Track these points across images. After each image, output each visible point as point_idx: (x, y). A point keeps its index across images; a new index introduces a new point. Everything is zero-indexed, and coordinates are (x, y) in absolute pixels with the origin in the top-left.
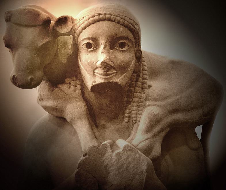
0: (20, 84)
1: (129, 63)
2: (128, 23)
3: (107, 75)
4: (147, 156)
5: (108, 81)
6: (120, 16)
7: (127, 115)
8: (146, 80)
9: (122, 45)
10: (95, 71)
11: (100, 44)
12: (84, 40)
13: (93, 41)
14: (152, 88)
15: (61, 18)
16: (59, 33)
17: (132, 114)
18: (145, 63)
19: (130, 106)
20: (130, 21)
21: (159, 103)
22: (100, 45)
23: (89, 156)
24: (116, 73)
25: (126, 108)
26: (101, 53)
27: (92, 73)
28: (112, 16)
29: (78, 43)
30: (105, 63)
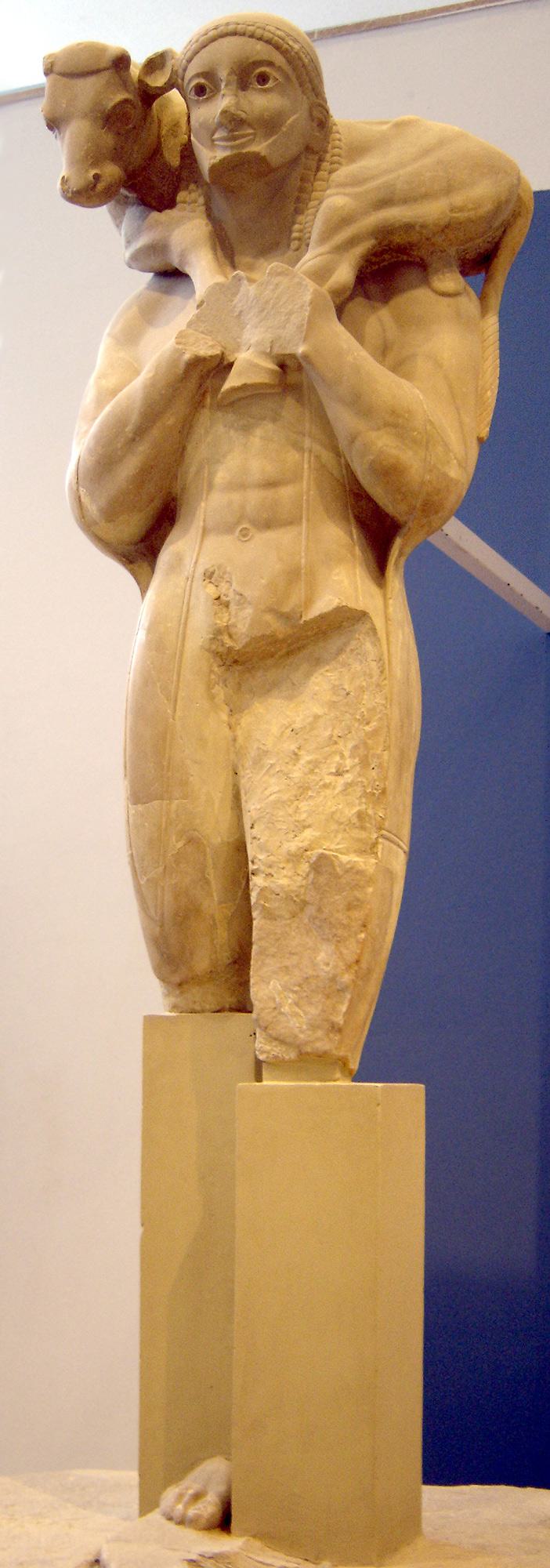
3: (234, 138)
5: (240, 151)
6: (257, 24)
9: (263, 79)
12: (190, 81)
13: (204, 78)
16: (151, 87)
21: (349, 190)
23: (208, 305)
24: (255, 134)
28: (240, 26)
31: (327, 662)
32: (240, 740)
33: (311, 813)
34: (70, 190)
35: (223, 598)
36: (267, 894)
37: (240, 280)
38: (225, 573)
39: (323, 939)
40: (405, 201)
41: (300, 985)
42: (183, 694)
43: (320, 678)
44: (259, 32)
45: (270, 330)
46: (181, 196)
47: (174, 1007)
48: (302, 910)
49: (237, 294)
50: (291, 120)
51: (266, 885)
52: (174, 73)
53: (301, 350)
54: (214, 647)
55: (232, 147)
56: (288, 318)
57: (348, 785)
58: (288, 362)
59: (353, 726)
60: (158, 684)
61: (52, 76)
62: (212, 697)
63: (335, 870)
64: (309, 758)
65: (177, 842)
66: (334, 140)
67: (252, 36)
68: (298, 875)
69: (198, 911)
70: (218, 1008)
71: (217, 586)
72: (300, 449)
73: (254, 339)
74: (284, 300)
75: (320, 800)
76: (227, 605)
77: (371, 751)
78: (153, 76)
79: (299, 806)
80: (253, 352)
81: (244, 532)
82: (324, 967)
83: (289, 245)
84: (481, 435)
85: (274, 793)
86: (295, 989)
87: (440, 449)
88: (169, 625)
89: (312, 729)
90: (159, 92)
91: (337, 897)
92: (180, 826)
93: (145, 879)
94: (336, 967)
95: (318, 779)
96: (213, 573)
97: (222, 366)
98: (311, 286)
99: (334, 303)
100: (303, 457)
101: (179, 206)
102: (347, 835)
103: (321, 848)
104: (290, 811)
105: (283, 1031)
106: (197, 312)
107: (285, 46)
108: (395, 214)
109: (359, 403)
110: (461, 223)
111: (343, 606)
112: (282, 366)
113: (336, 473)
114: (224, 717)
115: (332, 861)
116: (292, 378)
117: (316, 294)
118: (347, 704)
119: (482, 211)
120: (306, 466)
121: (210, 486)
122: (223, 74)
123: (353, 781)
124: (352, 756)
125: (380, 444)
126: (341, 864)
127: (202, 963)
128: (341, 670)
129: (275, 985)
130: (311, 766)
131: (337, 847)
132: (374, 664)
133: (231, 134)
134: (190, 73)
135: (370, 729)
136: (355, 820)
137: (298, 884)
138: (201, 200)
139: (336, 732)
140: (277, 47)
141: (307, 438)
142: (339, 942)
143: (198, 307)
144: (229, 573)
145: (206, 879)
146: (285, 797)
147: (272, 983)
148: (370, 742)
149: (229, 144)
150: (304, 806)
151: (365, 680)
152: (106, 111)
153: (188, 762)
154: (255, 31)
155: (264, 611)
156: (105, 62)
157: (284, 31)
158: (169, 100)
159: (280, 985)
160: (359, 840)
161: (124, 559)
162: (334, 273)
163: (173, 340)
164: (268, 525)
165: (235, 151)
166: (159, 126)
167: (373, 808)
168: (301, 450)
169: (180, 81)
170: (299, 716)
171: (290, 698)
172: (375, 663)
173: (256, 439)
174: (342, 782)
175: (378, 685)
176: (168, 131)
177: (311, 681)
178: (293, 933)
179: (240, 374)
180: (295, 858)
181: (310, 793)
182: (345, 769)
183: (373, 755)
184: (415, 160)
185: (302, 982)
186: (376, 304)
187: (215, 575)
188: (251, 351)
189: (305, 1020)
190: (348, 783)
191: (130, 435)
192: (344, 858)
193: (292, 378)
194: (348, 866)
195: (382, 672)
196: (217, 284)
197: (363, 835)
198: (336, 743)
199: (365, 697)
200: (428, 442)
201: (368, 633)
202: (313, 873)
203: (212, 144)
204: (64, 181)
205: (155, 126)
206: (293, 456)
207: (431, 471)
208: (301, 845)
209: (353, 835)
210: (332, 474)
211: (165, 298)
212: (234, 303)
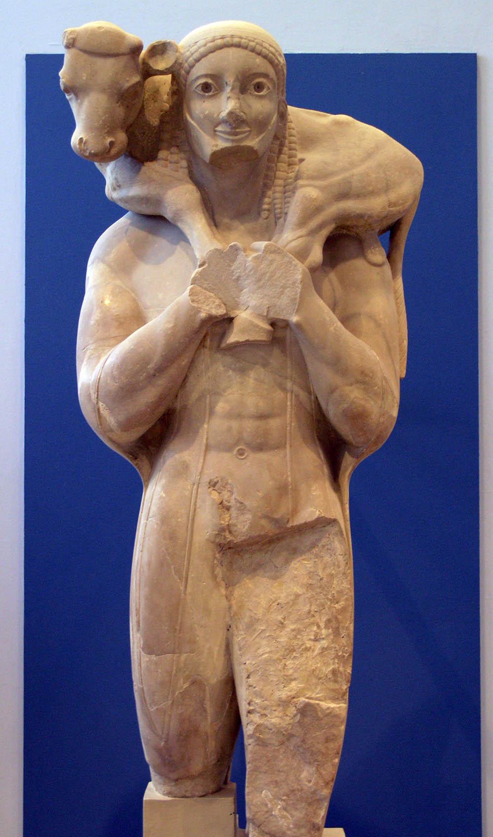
0: (93, 151)
1: (268, 118)
2: (268, 52)
3: (236, 134)
4: (303, 262)
5: (238, 144)
6: (256, 41)
8: (294, 151)
10: (216, 129)
11: (225, 84)
12: (198, 78)
14: (305, 161)
16: (153, 69)
17: (275, 204)
18: (293, 125)
19: (270, 193)
20: (271, 49)
22: (224, 87)
23: (209, 266)
24: (250, 131)
25: (263, 195)
26: (226, 99)
27: (212, 132)
29: (185, 85)
30: (234, 114)
31: (303, 553)
32: (234, 608)
33: (296, 670)
35: (225, 503)
36: (262, 728)
37: (237, 250)
38: (227, 484)
39: (306, 762)
40: (358, 196)
41: (288, 796)
42: (193, 575)
43: (298, 564)
44: (258, 48)
45: (266, 297)
46: (162, 154)
47: (169, 794)
48: (288, 740)
51: (262, 722)
53: (295, 319)
54: (218, 540)
55: (233, 141)
56: (282, 291)
57: (324, 649)
59: (327, 604)
62: (214, 577)
63: (317, 714)
64: (293, 627)
65: (184, 684)
66: (290, 129)
67: (253, 50)
68: (287, 715)
69: (196, 731)
70: (204, 793)
71: (219, 493)
73: (253, 302)
74: (278, 275)
75: (303, 660)
76: (228, 509)
77: (341, 625)
78: (154, 59)
79: (287, 664)
81: (241, 452)
82: (307, 783)
83: (259, 214)
86: (283, 798)
88: (179, 520)
89: (294, 604)
91: (318, 733)
92: (187, 673)
93: (155, 708)
94: (317, 783)
95: (300, 643)
96: (216, 483)
97: (228, 321)
102: (324, 687)
103: (304, 696)
104: (280, 667)
105: (274, 829)
108: (351, 206)
109: (338, 364)
111: (322, 517)
112: (273, 324)
114: (223, 591)
115: (315, 708)
118: (320, 587)
120: (289, 403)
121: (212, 413)
123: (328, 647)
124: (326, 627)
125: (352, 396)
126: (322, 710)
127: (197, 765)
128: (316, 560)
129: (266, 794)
130: (294, 633)
131: (318, 696)
133: (233, 130)
135: (340, 607)
136: (330, 676)
137: (287, 723)
138: (184, 163)
139: (314, 608)
141: (289, 380)
142: (318, 765)
144: (231, 484)
145: (204, 707)
146: (275, 657)
147: (264, 792)
148: (340, 617)
149: (231, 137)
150: (289, 662)
151: (334, 569)
153: (196, 626)
155: (261, 518)
156: (124, 49)
157: (274, 48)
159: (271, 794)
160: (333, 690)
161: (131, 456)
164: (260, 447)
165: (235, 144)
167: (344, 667)
168: (284, 389)
170: (282, 593)
171: (275, 578)
172: (342, 557)
173: (251, 379)
174: (319, 646)
175: (344, 574)
177: (290, 567)
178: (281, 757)
179: (243, 331)
180: (285, 703)
181: (295, 654)
182: (321, 637)
183: (343, 627)
184: (363, 161)
185: (289, 793)
189: (291, 821)
190: (324, 648)
191: (152, 372)
192: (325, 705)
193: (279, 334)
194: (328, 711)
195: (347, 563)
196: (216, 250)
197: (337, 686)
198: (313, 616)
199: (335, 582)
201: (337, 534)
202: (299, 715)
203: (214, 135)
206: (279, 395)
208: (289, 694)
209: (328, 686)
211: (150, 237)
212: (232, 268)
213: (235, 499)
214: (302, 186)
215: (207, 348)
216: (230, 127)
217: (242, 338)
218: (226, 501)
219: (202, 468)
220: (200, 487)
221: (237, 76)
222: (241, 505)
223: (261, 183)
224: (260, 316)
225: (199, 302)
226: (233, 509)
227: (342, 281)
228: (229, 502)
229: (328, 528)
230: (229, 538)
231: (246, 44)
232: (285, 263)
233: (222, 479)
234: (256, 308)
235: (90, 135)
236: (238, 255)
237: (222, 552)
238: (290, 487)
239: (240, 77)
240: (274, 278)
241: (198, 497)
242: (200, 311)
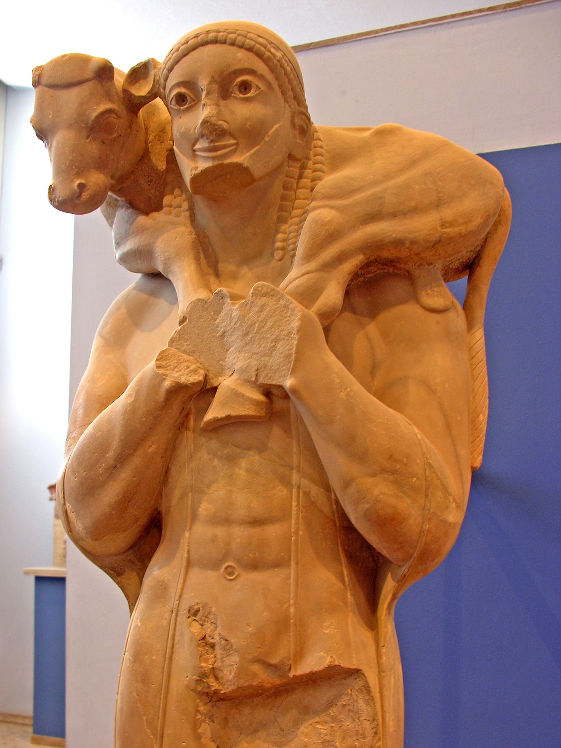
0: (60, 199)
3: (216, 149)
5: (221, 162)
6: (238, 32)
7: (278, 244)
12: (171, 90)
15: (138, 66)
16: (135, 97)
20: (260, 40)
24: (237, 144)
27: (191, 154)
28: (221, 34)
30: (209, 124)
31: (316, 713)
34: (56, 200)
35: (209, 639)
38: (210, 613)
40: (394, 215)
44: (240, 40)
45: (255, 356)
46: (167, 200)
49: (220, 312)
50: (275, 127)
52: (156, 82)
53: (288, 383)
54: (199, 688)
55: (214, 158)
58: (275, 391)
60: (144, 718)
61: (40, 88)
67: (233, 44)
71: (202, 625)
72: (286, 482)
73: (238, 365)
74: (269, 324)
76: (213, 646)
78: (137, 85)
80: (237, 379)
81: (230, 570)
83: (272, 255)
84: (475, 465)
85: (64, 504)
87: (440, 494)
88: (154, 657)
90: (143, 100)
96: (197, 611)
98: (298, 308)
99: (322, 325)
100: (292, 491)
101: (165, 210)
106: (179, 328)
107: (268, 54)
110: (451, 238)
111: (336, 666)
113: (326, 510)
116: (279, 404)
117: (305, 319)
119: (472, 226)
120: (294, 504)
121: (194, 516)
122: (203, 83)
128: (333, 725)
132: (367, 725)
133: (212, 145)
134: (171, 82)
138: (185, 205)
140: (259, 55)
143: (181, 322)
152: (90, 121)
154: (236, 39)
156: (92, 68)
158: (155, 107)
161: (112, 572)
162: (321, 293)
163: (153, 363)
165: (216, 163)
166: (147, 133)
169: (162, 90)
172: (369, 723)
176: (155, 137)
186: (364, 320)
187: (200, 614)
188: (235, 376)
191: (111, 462)
195: (376, 733)
196: (199, 300)
200: (427, 489)
201: (362, 691)
203: (193, 154)
204: (51, 190)
205: (142, 135)
206: (280, 492)
207: (429, 519)
210: (321, 511)
212: (217, 322)
213: (220, 634)
214: (314, 209)
215: (190, 431)
216: (207, 141)
217: (221, 414)
218: (210, 636)
219: (182, 589)
220: (179, 615)
221: (213, 77)
222: (226, 643)
223: (275, 216)
224: (247, 381)
225: (168, 368)
226: (217, 648)
227: (385, 335)
228: (212, 638)
229: (350, 681)
230: (215, 685)
231: (224, 37)
232: (280, 307)
233: (203, 607)
234: (243, 371)
235: (58, 180)
236: (224, 304)
237: (211, 704)
238: (292, 621)
239: (216, 77)
240: (264, 330)
241: (177, 629)
242: (164, 379)
